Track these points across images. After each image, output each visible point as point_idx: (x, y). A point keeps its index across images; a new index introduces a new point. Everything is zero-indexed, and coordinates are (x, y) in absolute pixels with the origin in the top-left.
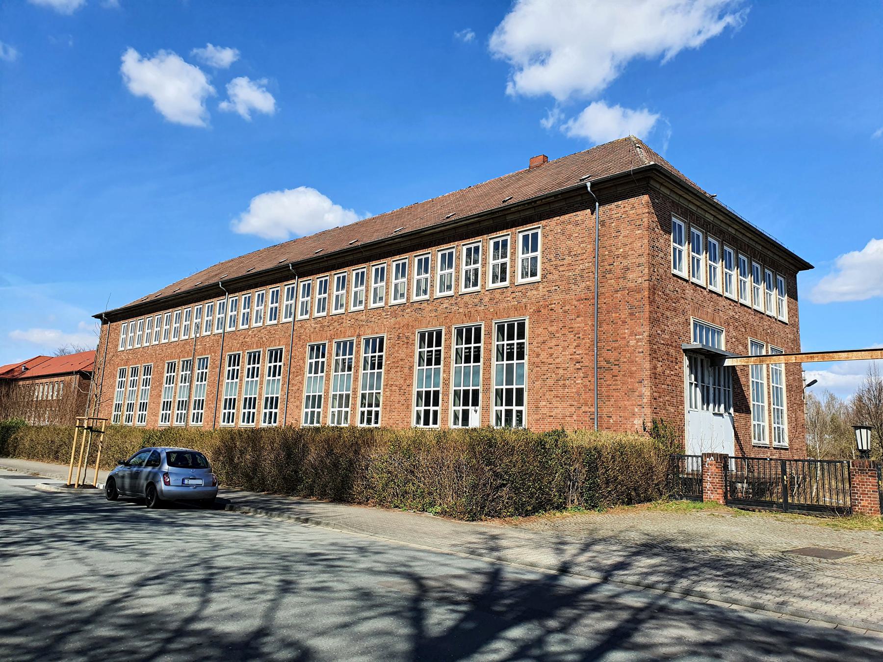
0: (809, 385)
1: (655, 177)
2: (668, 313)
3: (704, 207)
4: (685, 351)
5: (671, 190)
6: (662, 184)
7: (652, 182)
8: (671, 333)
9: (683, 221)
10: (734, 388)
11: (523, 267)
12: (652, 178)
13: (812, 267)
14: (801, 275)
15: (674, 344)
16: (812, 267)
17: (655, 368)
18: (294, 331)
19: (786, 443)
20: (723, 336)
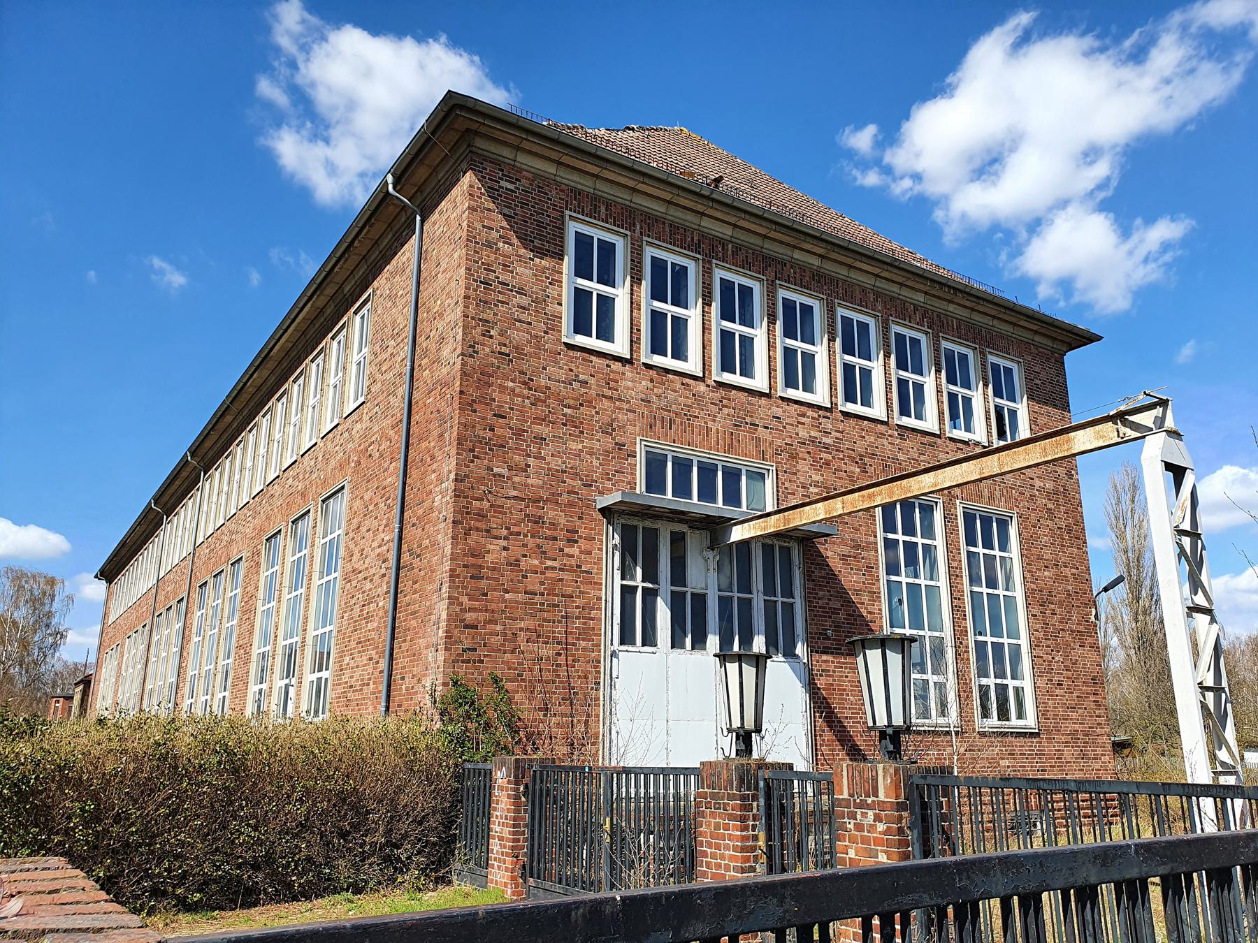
0: (1106, 589)
1: (483, 129)
2: (544, 430)
3: (886, 274)
4: (606, 512)
5: (559, 163)
6: (518, 148)
7: (480, 143)
8: (552, 473)
9: (1012, 360)
10: (811, 599)
11: (933, 565)
12: (476, 133)
13: (1099, 338)
14: (1070, 358)
15: (565, 498)
16: (1099, 338)
17: (477, 553)
18: (1106, 856)
19: (1030, 721)
20: (769, 483)
